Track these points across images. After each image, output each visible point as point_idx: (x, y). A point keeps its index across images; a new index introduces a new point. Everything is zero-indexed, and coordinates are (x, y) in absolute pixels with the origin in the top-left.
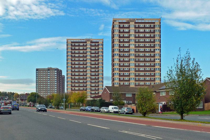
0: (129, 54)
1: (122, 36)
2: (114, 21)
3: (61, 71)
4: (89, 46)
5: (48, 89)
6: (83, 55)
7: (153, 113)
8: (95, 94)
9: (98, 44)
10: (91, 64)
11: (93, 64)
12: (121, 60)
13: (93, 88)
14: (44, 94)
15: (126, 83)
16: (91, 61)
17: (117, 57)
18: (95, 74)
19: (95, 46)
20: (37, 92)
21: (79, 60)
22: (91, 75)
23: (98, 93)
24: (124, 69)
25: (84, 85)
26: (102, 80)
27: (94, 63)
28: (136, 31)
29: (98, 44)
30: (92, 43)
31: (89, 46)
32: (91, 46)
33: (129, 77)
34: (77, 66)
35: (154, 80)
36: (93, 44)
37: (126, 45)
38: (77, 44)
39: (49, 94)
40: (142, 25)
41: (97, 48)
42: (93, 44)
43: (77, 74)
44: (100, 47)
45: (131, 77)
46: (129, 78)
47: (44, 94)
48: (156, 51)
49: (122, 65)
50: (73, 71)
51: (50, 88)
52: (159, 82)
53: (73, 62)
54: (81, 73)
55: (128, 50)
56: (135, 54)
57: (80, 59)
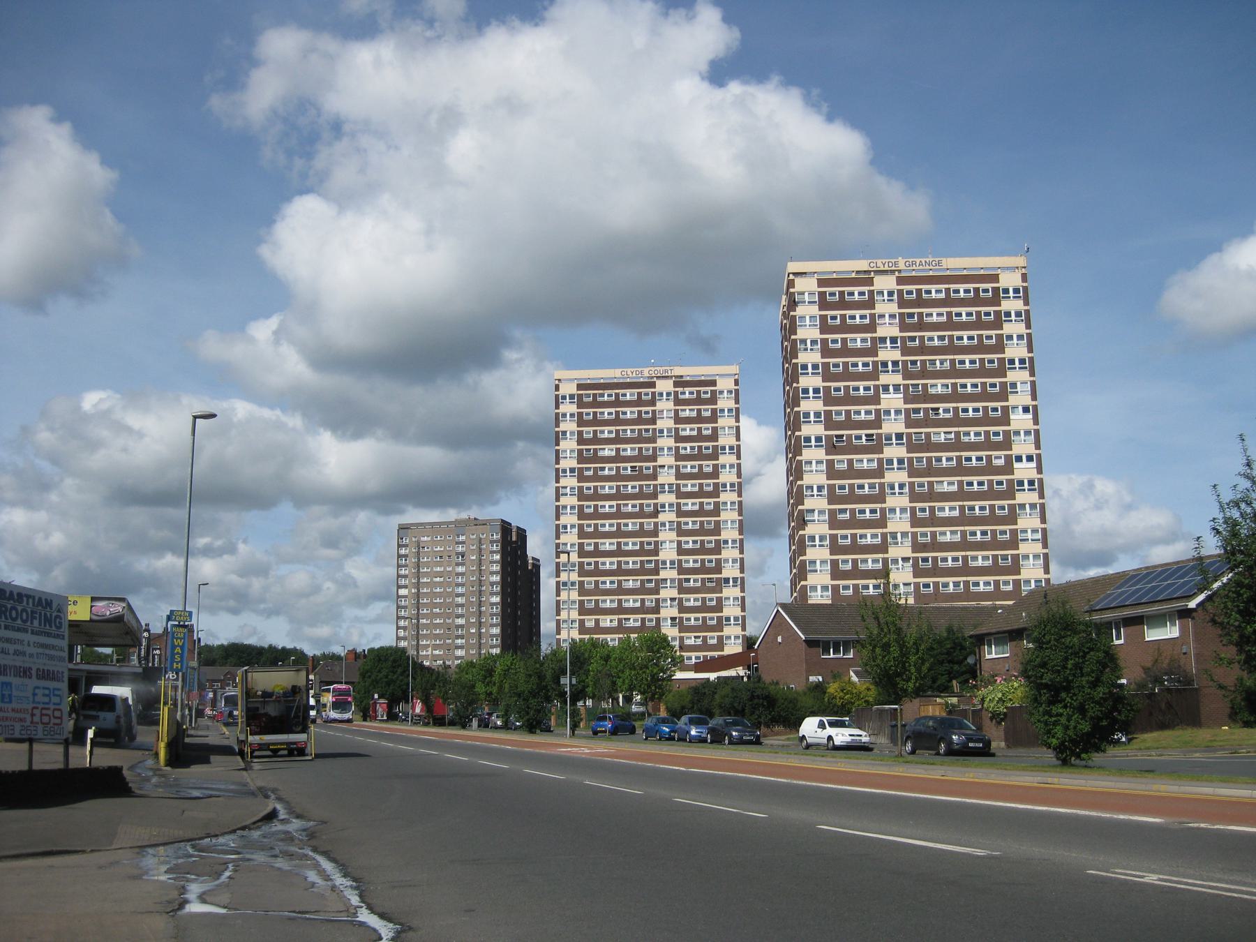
1: (843, 418)
2: (791, 277)
3: (522, 534)
5: (458, 605)
8: (705, 646)
11: (688, 420)
12: (842, 567)
14: (437, 652)
15: (861, 461)
17: (813, 454)
18: (699, 429)
19: (699, 401)
20: (403, 644)
21: (620, 590)
22: (681, 551)
23: (720, 645)
24: (850, 462)
25: (647, 604)
26: (739, 595)
27: (694, 414)
30: (680, 390)
32: (679, 554)
33: (881, 556)
35: (1015, 568)
39: (459, 653)
40: (935, 291)
41: (708, 414)
42: (687, 390)
43: (607, 547)
44: (722, 422)
47: (437, 652)
48: (1016, 465)
49: (849, 567)
51: (468, 610)
52: (1040, 574)
53: (588, 433)
55: (872, 417)
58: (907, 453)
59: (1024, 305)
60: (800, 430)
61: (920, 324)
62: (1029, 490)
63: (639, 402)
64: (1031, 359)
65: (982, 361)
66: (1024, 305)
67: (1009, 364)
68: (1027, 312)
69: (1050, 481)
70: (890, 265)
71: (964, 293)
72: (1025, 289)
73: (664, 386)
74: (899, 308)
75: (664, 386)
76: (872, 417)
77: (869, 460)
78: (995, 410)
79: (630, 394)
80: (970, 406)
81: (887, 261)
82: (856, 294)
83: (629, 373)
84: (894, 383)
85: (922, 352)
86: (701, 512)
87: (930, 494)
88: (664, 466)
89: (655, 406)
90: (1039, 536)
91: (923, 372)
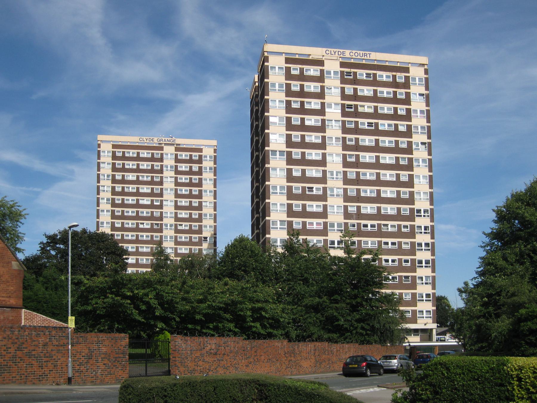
0: (325, 224)
4: (169, 161)
6: (153, 154)
7: (468, 284)
9: (200, 157)
10: (177, 184)
13: (184, 177)
16: (177, 172)
28: (349, 160)
29: (200, 157)
31: (169, 161)
34: (130, 212)
36: (184, 155)
37: (315, 209)
38: (132, 153)
45: (328, 133)
46: (324, 138)
50: (117, 225)
54: (143, 176)
55: (321, 227)
56: (342, 73)
57: (141, 202)
58: (344, 219)
59: (431, 222)
60: (268, 79)
61: (358, 181)
62: (426, 300)
63: (152, 159)
64: (433, 260)
65: (400, 260)
66: (431, 222)
67: (417, 213)
68: (433, 260)
69: (440, 228)
70: (340, 53)
71: (386, 78)
72: (430, 144)
73: (169, 150)
74: (342, 117)
75: (169, 150)
76: (321, 227)
77: (317, 206)
78: (406, 261)
79: (145, 154)
80: (390, 240)
81: (337, 50)
82: (315, 224)
83: (145, 139)
84: (335, 102)
85: (358, 200)
86: (190, 219)
87: (358, 198)
88: (168, 200)
89: (163, 162)
90: (430, 281)
91: (359, 232)
